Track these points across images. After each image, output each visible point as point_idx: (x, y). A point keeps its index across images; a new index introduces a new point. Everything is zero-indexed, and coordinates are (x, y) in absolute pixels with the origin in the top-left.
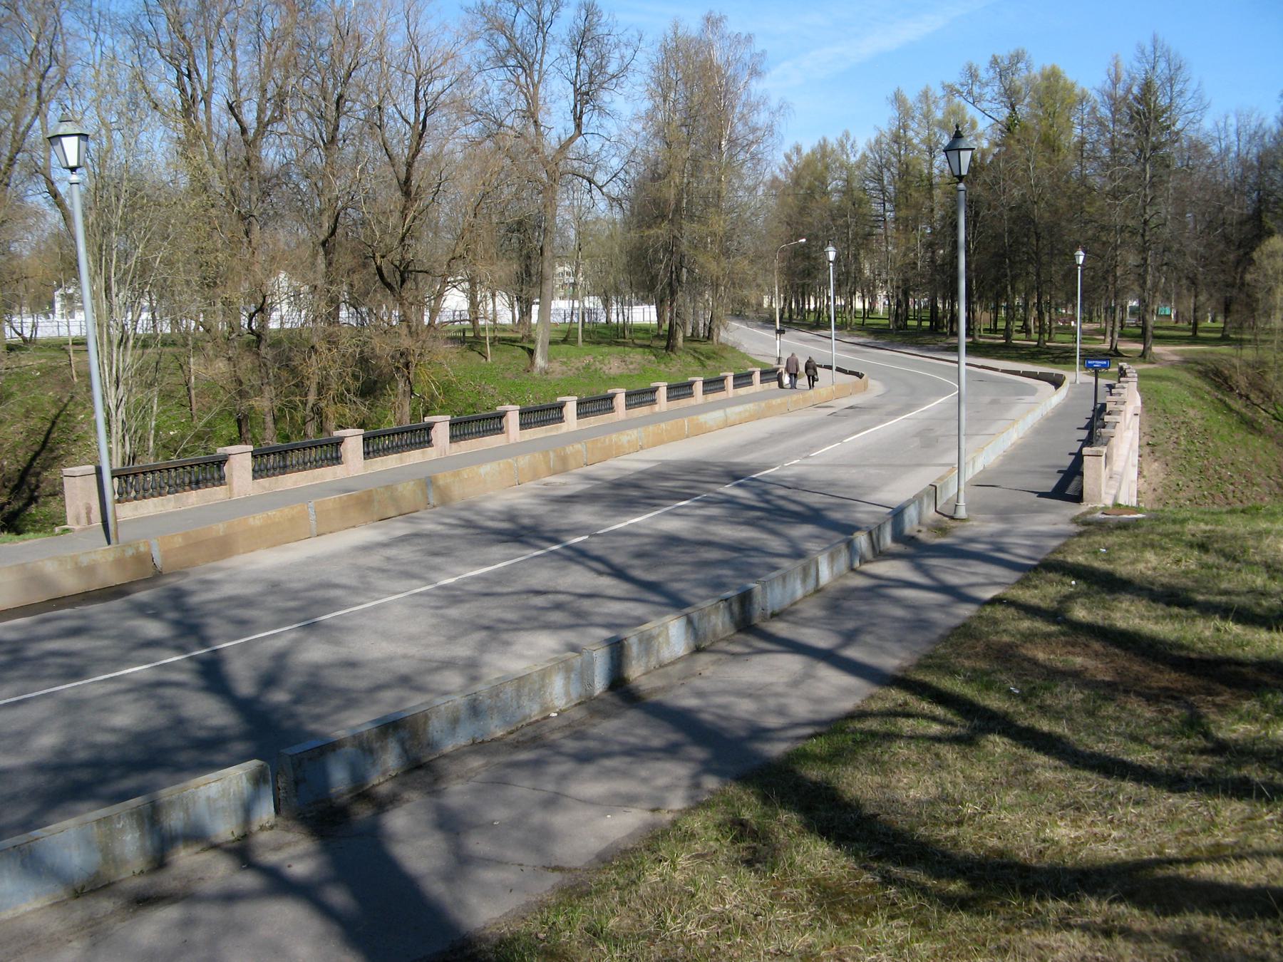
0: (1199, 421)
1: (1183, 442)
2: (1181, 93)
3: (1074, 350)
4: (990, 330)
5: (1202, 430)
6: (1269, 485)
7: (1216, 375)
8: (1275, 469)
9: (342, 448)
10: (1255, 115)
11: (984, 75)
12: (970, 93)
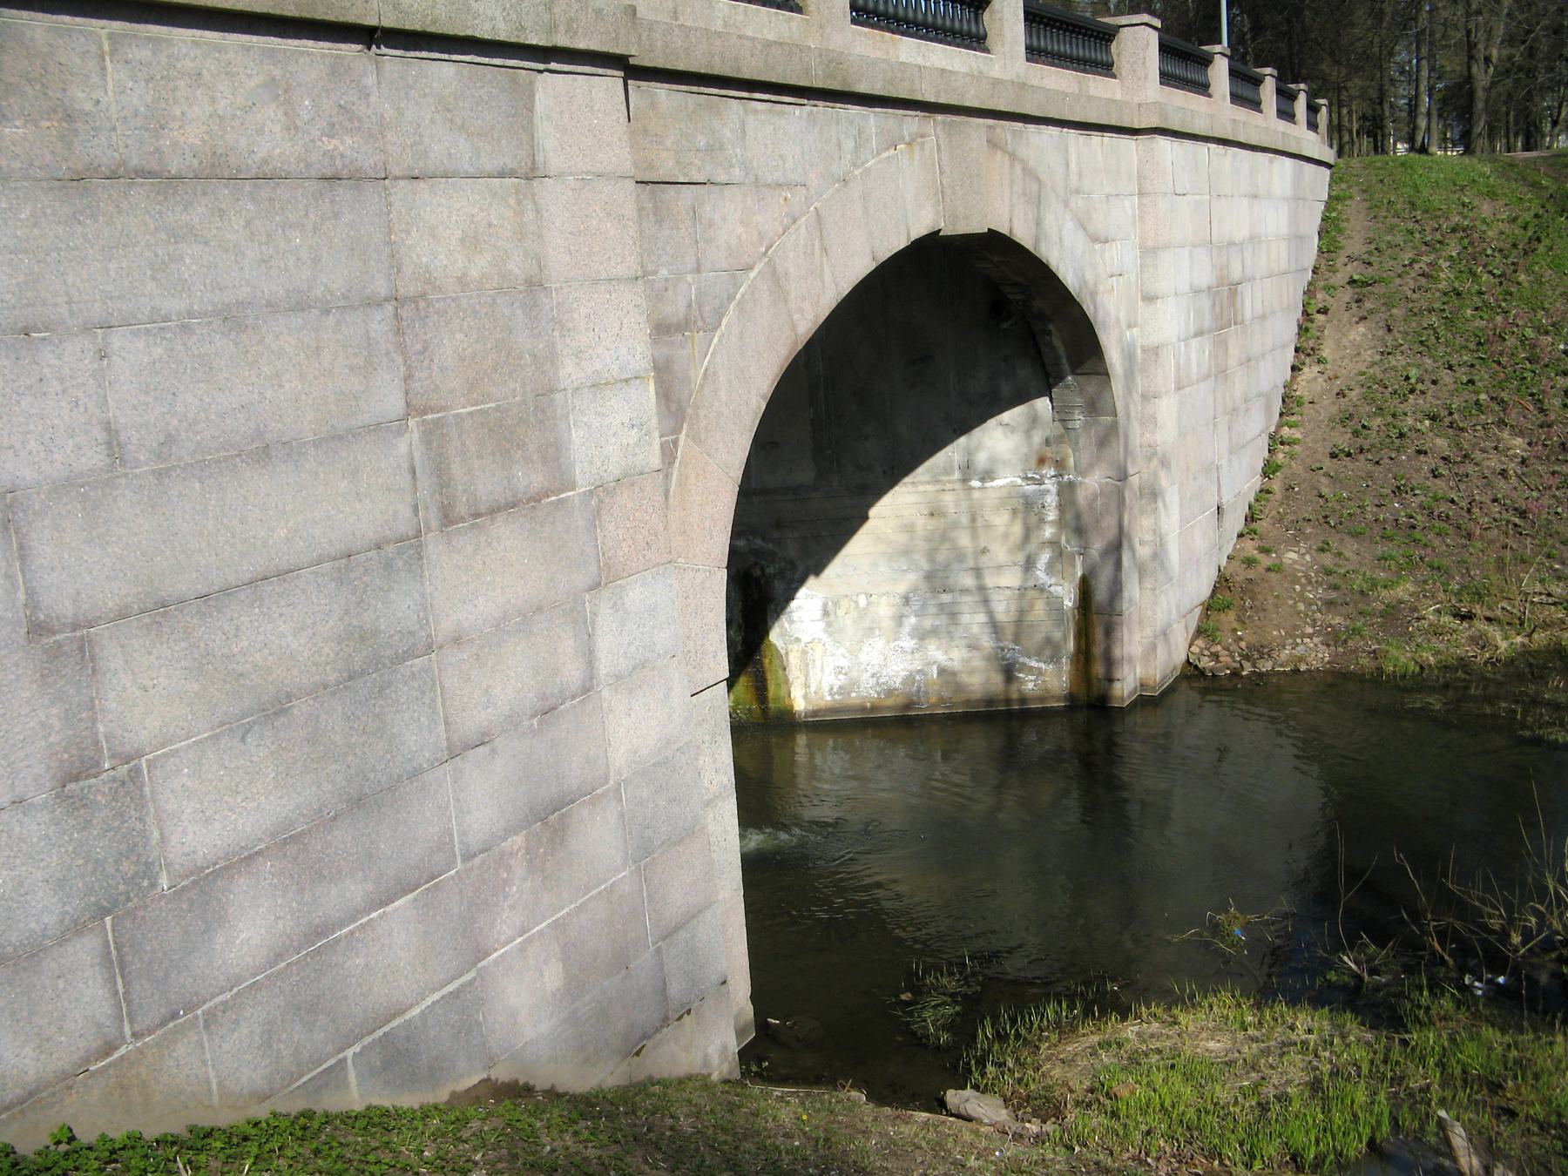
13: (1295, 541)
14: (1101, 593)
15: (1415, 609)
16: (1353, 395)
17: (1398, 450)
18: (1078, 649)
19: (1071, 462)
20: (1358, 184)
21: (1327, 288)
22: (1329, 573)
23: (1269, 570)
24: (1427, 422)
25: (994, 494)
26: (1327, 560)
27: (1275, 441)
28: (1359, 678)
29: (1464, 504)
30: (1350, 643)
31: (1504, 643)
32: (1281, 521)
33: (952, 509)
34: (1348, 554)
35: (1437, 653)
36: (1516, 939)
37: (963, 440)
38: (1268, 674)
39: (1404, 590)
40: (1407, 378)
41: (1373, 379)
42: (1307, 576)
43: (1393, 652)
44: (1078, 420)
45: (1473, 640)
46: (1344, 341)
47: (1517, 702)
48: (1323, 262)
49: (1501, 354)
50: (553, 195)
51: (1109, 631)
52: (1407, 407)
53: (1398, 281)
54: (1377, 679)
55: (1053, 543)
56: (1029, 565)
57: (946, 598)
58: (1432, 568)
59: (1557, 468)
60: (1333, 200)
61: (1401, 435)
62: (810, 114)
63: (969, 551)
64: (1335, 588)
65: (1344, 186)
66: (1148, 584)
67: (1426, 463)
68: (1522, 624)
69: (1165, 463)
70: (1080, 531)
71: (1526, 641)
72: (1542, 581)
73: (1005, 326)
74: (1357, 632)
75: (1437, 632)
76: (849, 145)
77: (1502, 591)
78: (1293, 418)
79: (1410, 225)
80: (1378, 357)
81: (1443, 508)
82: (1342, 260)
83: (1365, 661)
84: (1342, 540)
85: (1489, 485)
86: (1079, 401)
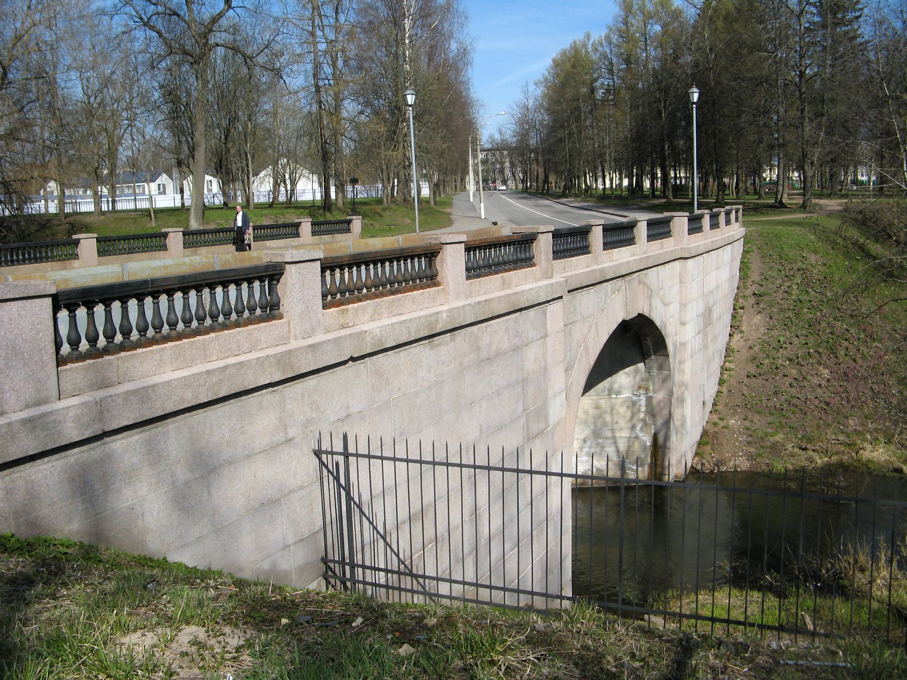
9: (300, 229)
13: (733, 415)
14: (661, 439)
15: (783, 446)
16: (756, 348)
17: (775, 375)
18: (652, 462)
19: (651, 388)
20: (756, 244)
21: (744, 297)
22: (748, 429)
23: (723, 427)
24: (788, 362)
25: (621, 400)
26: (747, 423)
27: (723, 369)
28: (761, 474)
29: (803, 399)
30: (758, 460)
31: (820, 461)
32: (727, 406)
33: (604, 406)
34: (755, 421)
35: (793, 464)
36: (824, 572)
37: (609, 379)
38: (725, 472)
39: (779, 437)
40: (779, 341)
41: (764, 341)
42: (739, 431)
43: (775, 464)
44: (655, 372)
45: (807, 459)
46: (752, 323)
47: (825, 486)
48: (742, 284)
49: (819, 331)
50: (549, 340)
51: (664, 454)
52: (779, 354)
53: (774, 294)
54: (770, 475)
55: (644, 420)
56: (633, 428)
57: (601, 441)
58: (790, 428)
59: (842, 384)
60: (745, 252)
61: (777, 368)
62: (595, 290)
63: (610, 423)
64: (751, 436)
65: (750, 245)
66: (679, 436)
67: (788, 381)
68: (827, 452)
69: (686, 388)
70: (653, 416)
71: (829, 460)
72: (835, 434)
73: (628, 335)
74: (759, 455)
75: (793, 455)
76: (604, 297)
77: (819, 438)
78: (730, 359)
79: (780, 267)
80: (766, 331)
81: (795, 401)
82: (750, 283)
83: (764, 467)
84: (753, 415)
85: (814, 391)
86: (656, 365)
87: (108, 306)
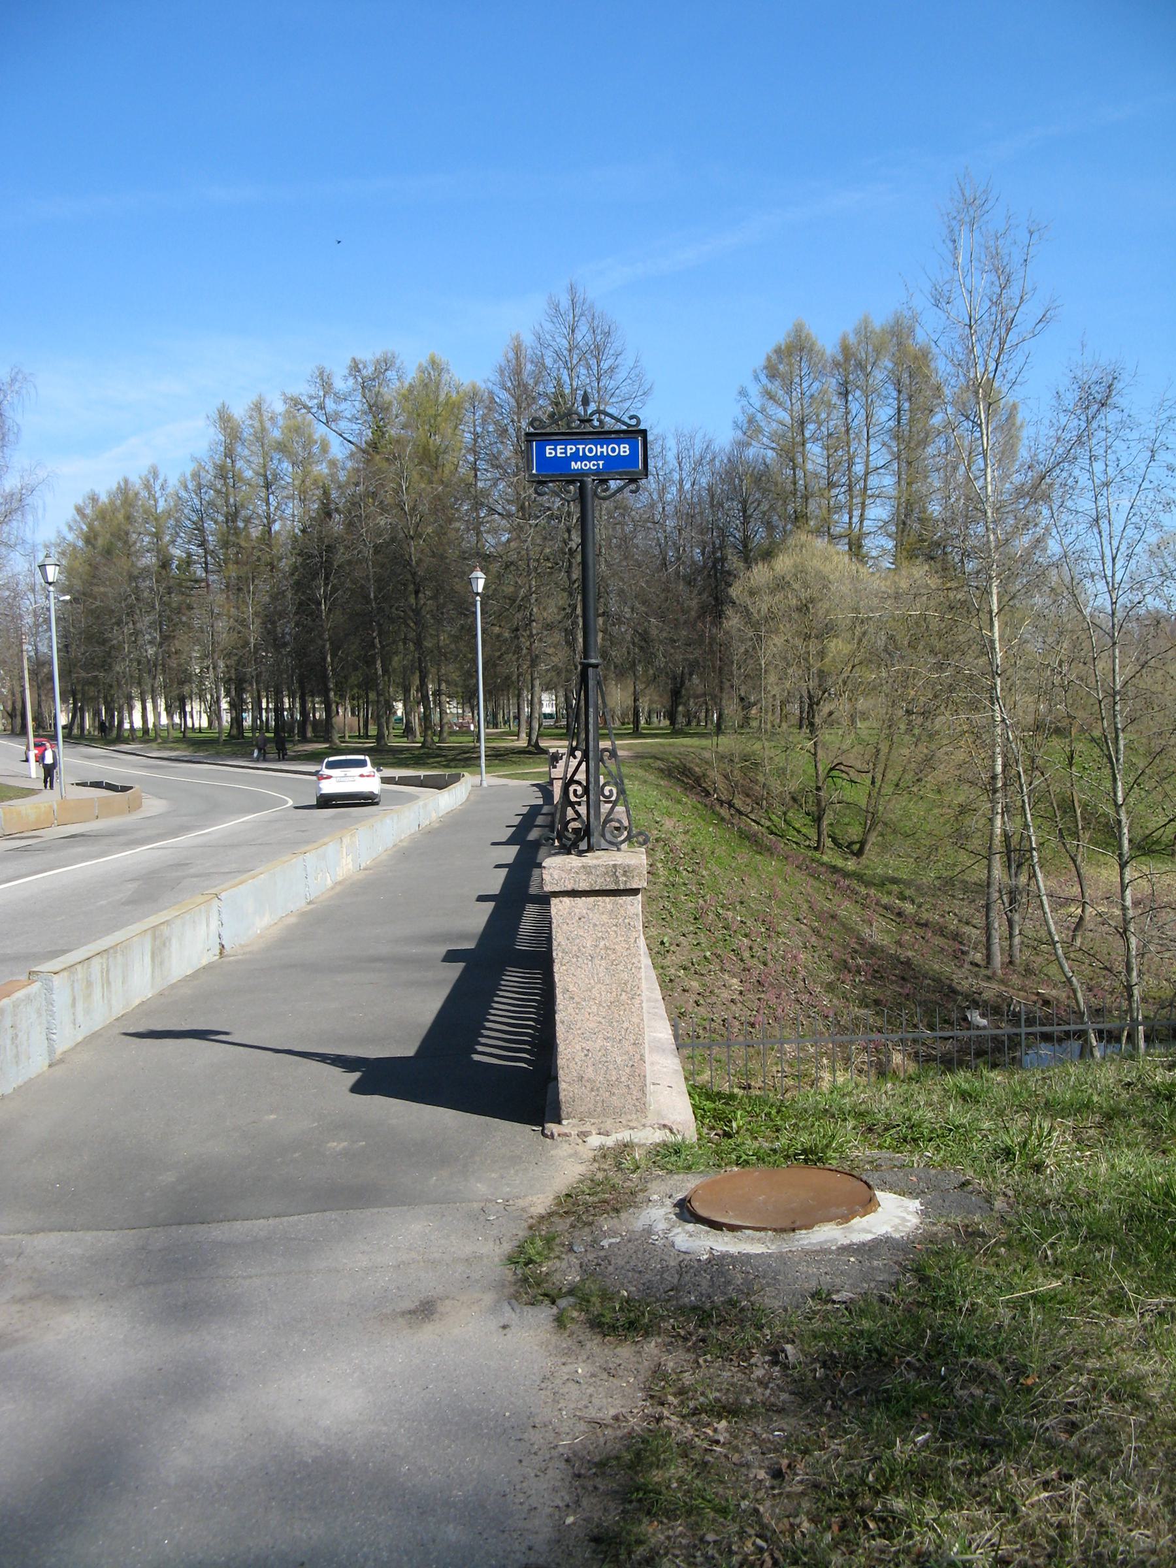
0: (682, 837)
1: (661, 872)
2: (612, 369)
3: (476, 750)
4: (359, 737)
5: (688, 849)
6: (800, 933)
7: (683, 774)
8: (805, 906)
10: (699, 436)
11: (341, 384)
12: (321, 407)
40: (662, 943)
61: (671, 981)
87: (132, 728)
